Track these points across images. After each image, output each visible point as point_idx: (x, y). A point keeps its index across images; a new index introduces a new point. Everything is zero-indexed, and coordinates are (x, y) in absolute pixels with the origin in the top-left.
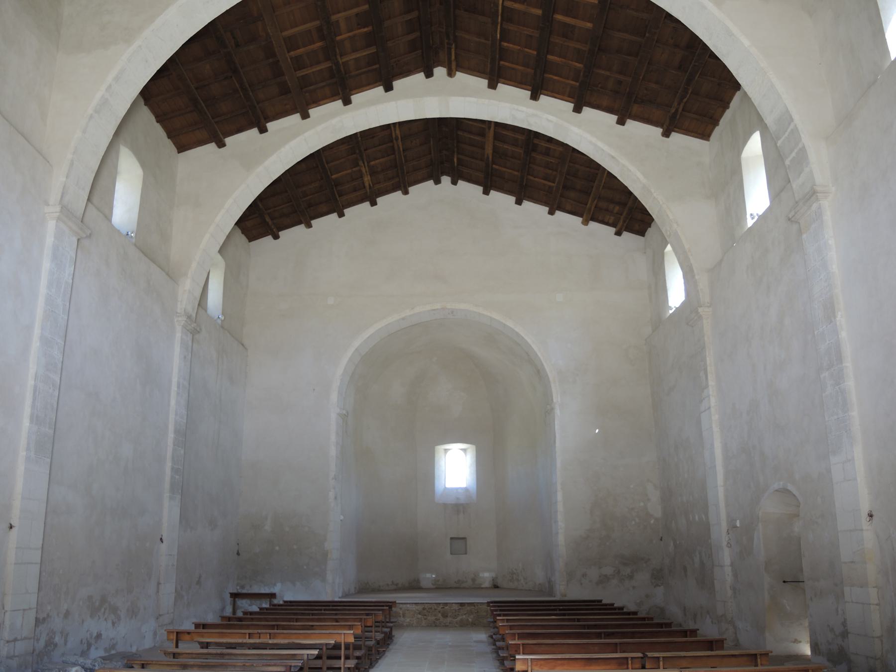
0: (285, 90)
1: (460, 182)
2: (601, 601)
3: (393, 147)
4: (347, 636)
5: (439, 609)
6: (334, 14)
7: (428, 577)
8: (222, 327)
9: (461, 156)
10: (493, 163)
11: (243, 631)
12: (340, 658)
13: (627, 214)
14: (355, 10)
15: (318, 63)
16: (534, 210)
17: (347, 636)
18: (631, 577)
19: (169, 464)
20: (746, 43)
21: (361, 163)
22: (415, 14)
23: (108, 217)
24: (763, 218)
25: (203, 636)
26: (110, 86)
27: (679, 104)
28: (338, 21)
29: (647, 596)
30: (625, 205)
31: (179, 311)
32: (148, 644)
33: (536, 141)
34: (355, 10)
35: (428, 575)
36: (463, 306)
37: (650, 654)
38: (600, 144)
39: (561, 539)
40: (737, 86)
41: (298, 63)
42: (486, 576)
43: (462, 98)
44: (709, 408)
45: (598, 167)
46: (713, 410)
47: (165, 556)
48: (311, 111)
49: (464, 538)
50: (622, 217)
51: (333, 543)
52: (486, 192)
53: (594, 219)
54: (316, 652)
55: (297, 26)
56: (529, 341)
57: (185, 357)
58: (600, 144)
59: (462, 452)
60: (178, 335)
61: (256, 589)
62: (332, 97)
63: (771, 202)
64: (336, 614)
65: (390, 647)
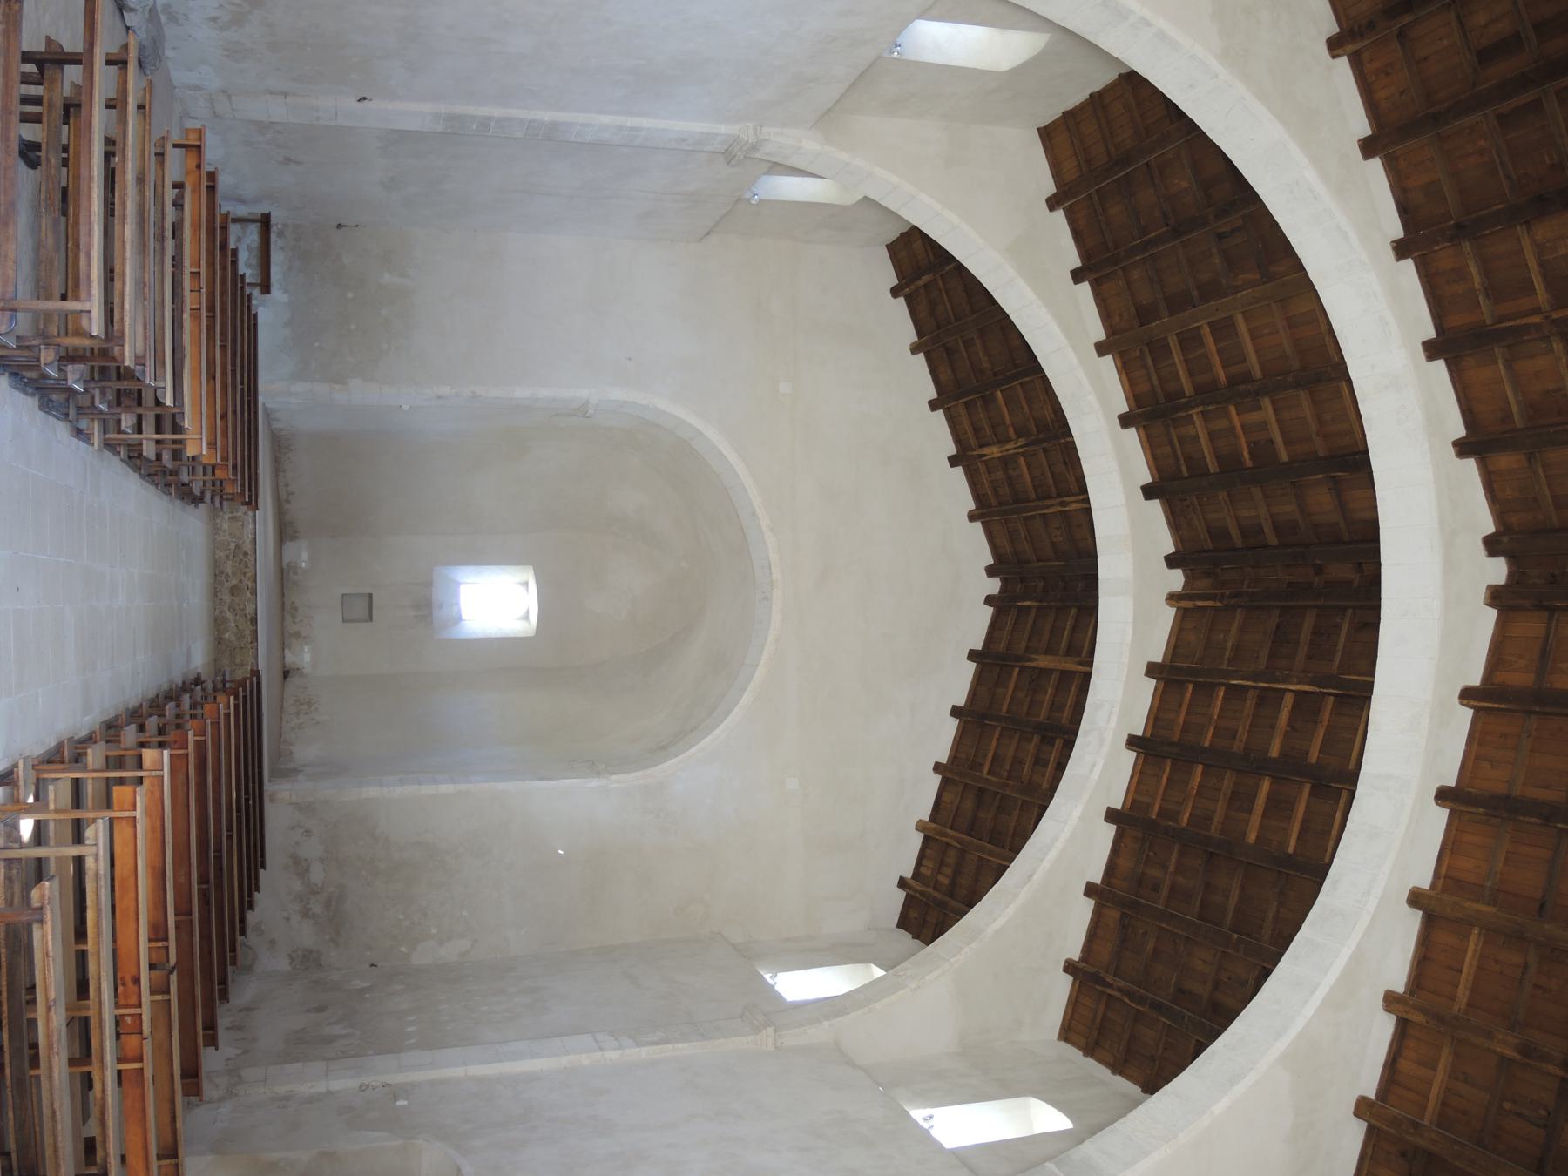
0: (1144, 315)
1: (991, 610)
2: (263, 867)
3: (1050, 498)
4: (197, 443)
5: (246, 581)
6: (1273, 402)
7: (300, 554)
8: (739, 200)
9: (1033, 612)
10: (1022, 669)
11: (203, 263)
12: (158, 431)
13: (935, 901)
14: (1278, 439)
15: (1191, 374)
16: (942, 737)
17: (197, 443)
18: (306, 914)
19: (496, 112)
20: (1219, 1108)
21: (1022, 442)
22: (1272, 540)
23: (925, 14)
24: (925, 1137)
25: (193, 191)
26: (1149, 24)
27: (1119, 989)
28: (1260, 408)
29: (273, 942)
30: (951, 895)
31: (765, 130)
32: (179, 76)
33: (1059, 743)
34: (1278, 439)
35: (305, 556)
36: (776, 617)
37: (174, 977)
38: (1053, 855)
39: (372, 792)
40: (1151, 1087)
41: (1190, 340)
42: (302, 657)
43: (1131, 619)
44: (601, 1049)
45: (1016, 850)
46: (598, 1054)
47: (335, 106)
48: (1109, 359)
49: (371, 618)
50: (930, 890)
51: (361, 393)
52: (973, 655)
53: (927, 841)
54: (169, 402)
55: (1253, 338)
56: (716, 732)
57: (683, 140)
58: (1053, 855)
59: (522, 612)
60: (723, 129)
61: (276, 257)
62: (1134, 396)
63: (954, 1152)
64: (235, 412)
65: (178, 502)
